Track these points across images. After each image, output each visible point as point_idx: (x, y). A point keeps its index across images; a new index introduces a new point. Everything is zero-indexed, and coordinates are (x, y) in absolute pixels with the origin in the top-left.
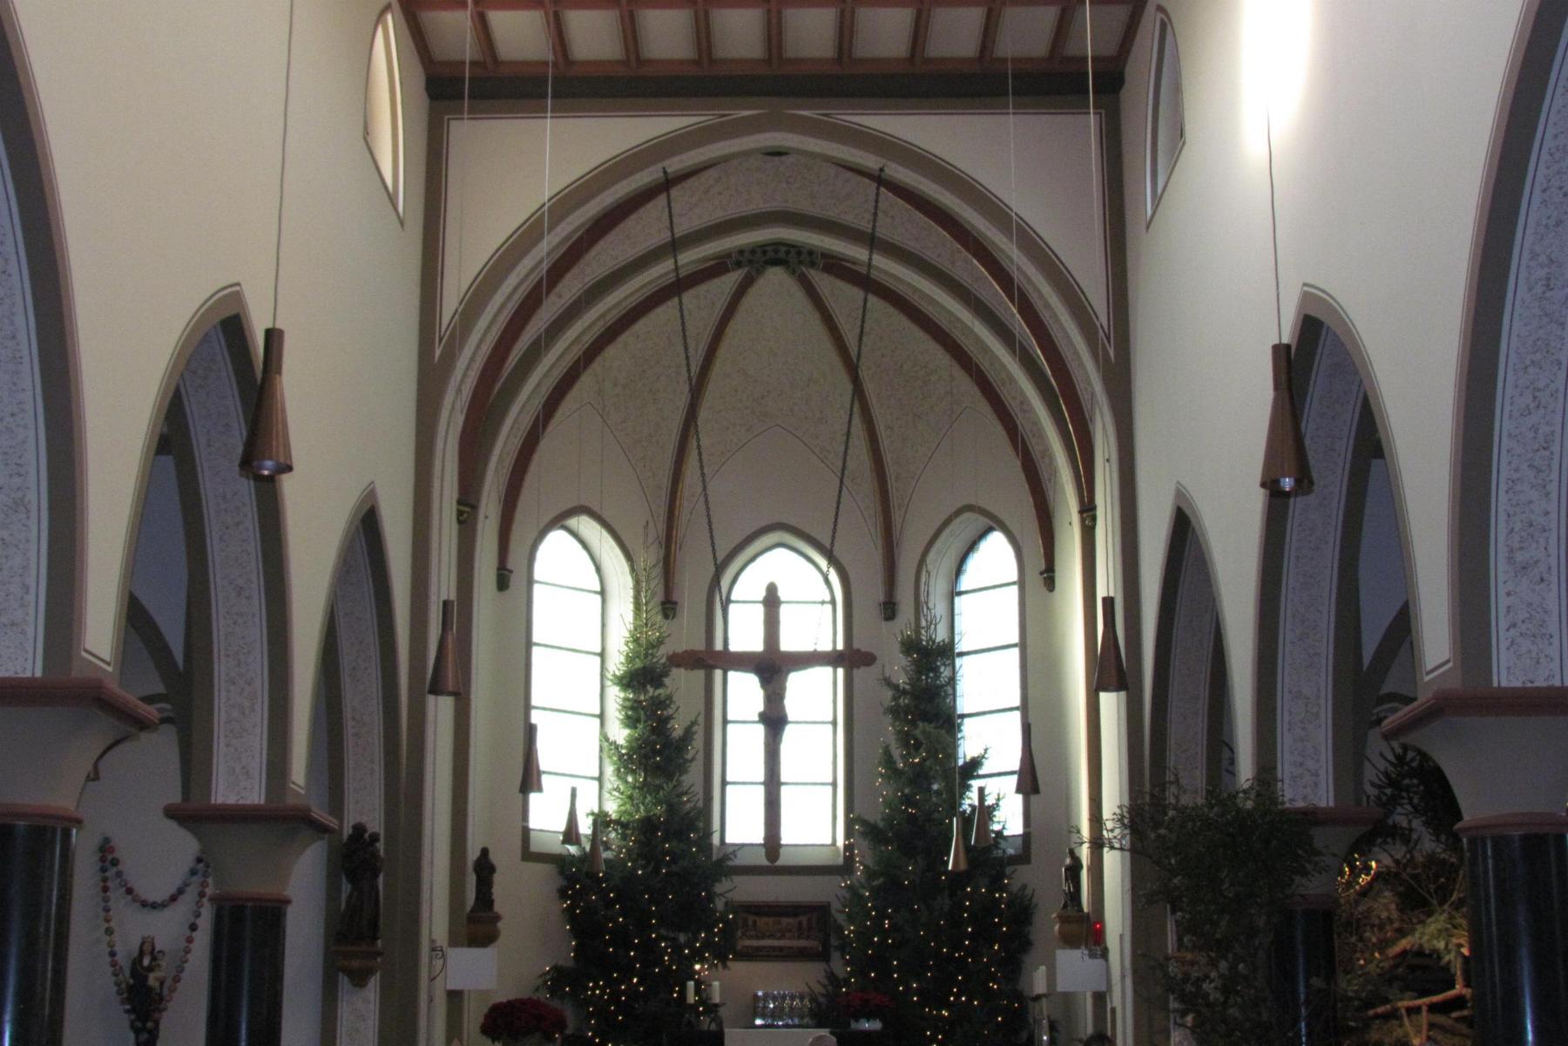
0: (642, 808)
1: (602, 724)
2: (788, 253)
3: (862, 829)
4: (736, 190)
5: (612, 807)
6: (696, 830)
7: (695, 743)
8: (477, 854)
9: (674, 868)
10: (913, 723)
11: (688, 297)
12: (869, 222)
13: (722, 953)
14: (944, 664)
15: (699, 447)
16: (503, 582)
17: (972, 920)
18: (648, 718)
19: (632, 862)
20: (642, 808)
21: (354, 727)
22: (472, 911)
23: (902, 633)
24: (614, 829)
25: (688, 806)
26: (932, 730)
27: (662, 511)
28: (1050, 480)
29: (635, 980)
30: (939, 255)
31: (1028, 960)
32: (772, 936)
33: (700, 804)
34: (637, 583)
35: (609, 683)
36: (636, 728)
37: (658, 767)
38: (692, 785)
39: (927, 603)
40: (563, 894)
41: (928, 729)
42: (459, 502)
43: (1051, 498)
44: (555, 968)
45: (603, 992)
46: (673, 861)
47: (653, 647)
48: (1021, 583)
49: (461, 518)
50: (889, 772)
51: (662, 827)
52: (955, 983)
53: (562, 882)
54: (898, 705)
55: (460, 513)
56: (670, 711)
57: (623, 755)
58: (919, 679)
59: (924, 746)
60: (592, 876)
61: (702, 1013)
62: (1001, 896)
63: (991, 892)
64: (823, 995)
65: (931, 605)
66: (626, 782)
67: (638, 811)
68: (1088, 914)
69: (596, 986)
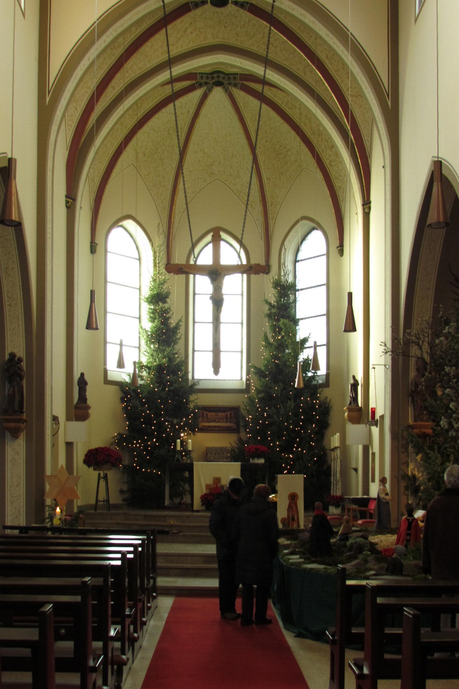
0: (157, 360)
1: (140, 322)
2: (224, 78)
3: (254, 371)
4: (200, 31)
5: (145, 360)
6: (181, 371)
7: (180, 330)
8: (79, 376)
9: (172, 388)
10: (278, 320)
11: (178, 102)
12: (264, 50)
13: (193, 428)
14: (291, 294)
15: (184, 181)
16: (93, 249)
17: (304, 413)
18: (160, 317)
19: (152, 385)
20: (157, 360)
21: (8, 301)
22: (77, 404)
23: (273, 278)
24: (145, 370)
25: (178, 360)
26: (287, 322)
27: (166, 220)
28: (343, 201)
29: (154, 440)
30: (298, 69)
31: (328, 432)
32: (214, 421)
33: (183, 359)
34: (155, 253)
35: (142, 301)
36: (154, 322)
37: (163, 341)
38: (180, 349)
39: (284, 264)
40: (122, 400)
41: (285, 322)
42: (67, 197)
43: (343, 210)
44: (119, 434)
45: (140, 446)
46: (171, 385)
47: (162, 284)
48: (328, 254)
49: (68, 205)
50: (267, 344)
51: (166, 369)
52: (296, 442)
53: (123, 395)
54: (271, 313)
55: (67, 202)
56: (170, 315)
57: (149, 335)
58: (281, 301)
59: (283, 330)
60: (135, 391)
61: (184, 456)
62: (316, 402)
63: (312, 400)
64: (237, 448)
65: (286, 265)
66: (150, 348)
67: (155, 361)
68: (361, 408)
69: (138, 443)
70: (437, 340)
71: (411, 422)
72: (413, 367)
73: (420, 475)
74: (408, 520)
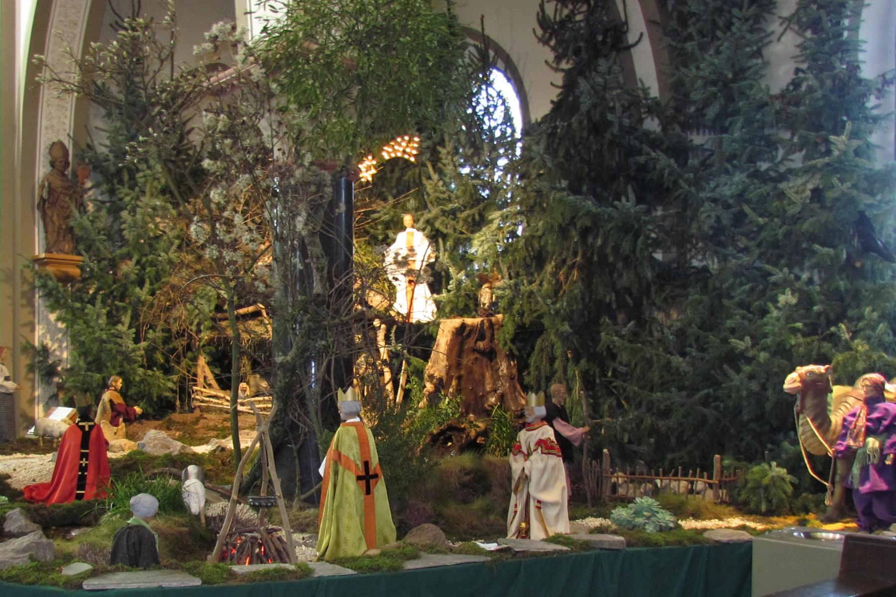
70: (195, 47)
71: (39, 251)
72: (42, 159)
73: (56, 346)
74: (82, 428)
